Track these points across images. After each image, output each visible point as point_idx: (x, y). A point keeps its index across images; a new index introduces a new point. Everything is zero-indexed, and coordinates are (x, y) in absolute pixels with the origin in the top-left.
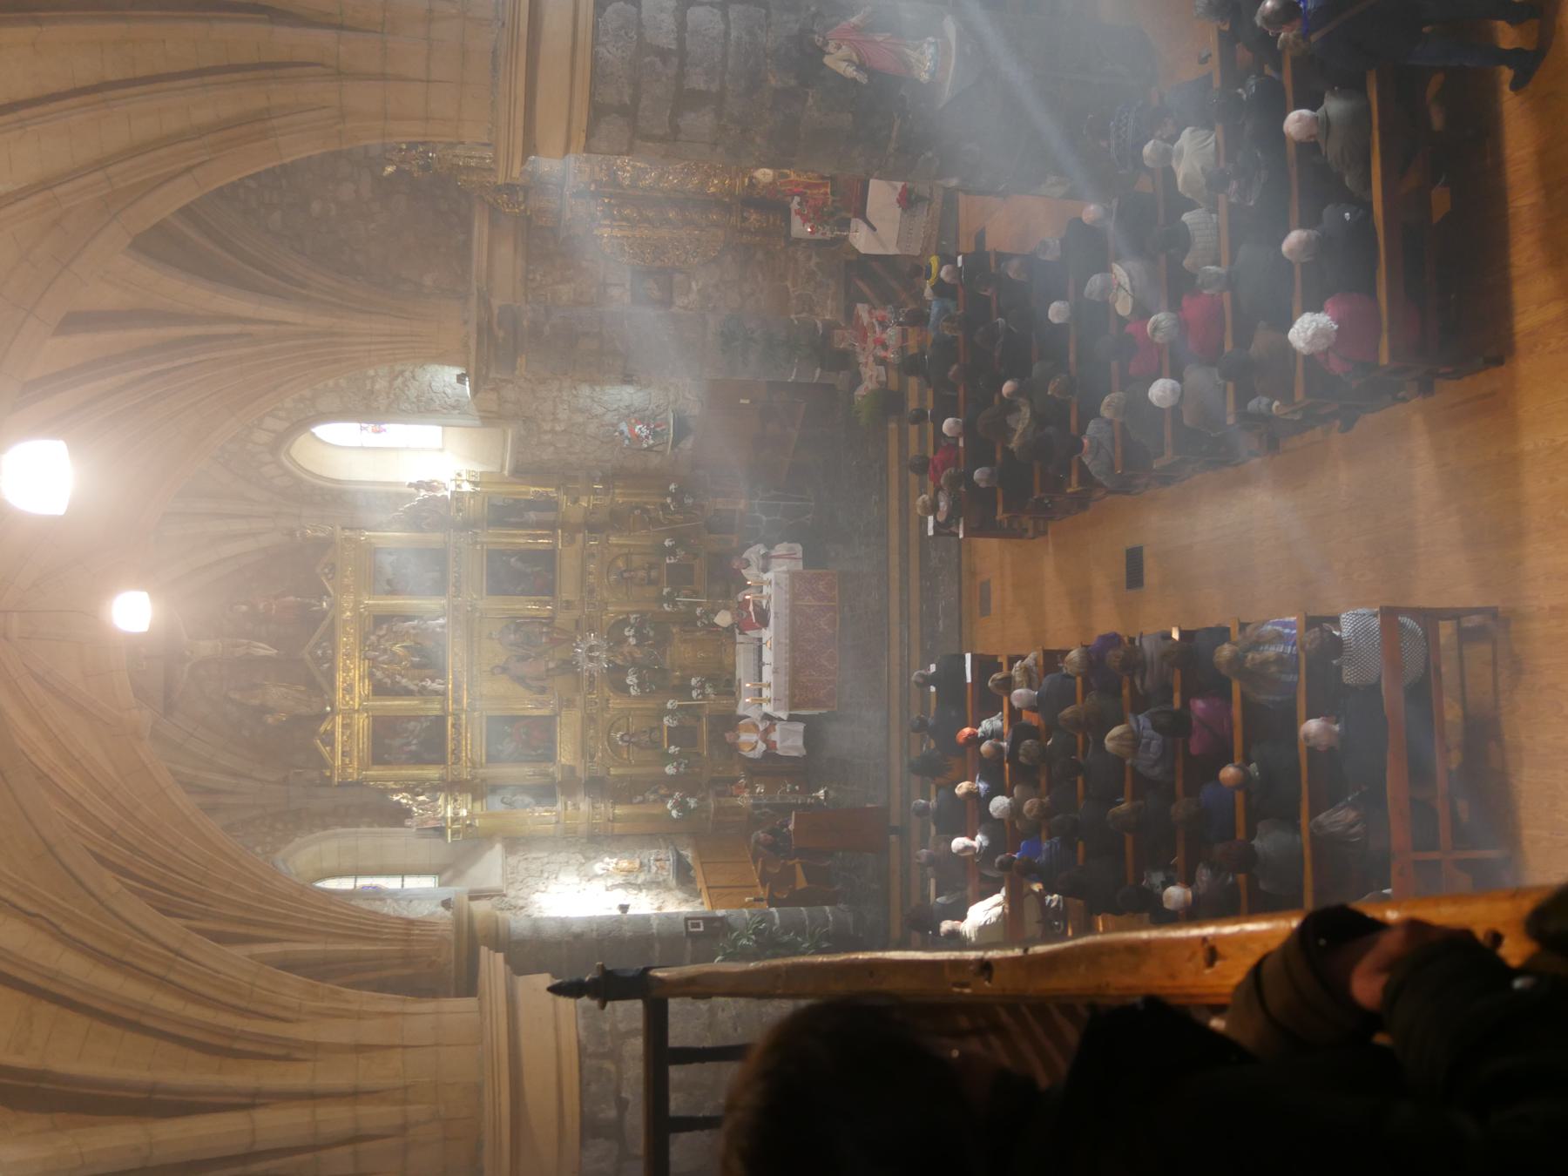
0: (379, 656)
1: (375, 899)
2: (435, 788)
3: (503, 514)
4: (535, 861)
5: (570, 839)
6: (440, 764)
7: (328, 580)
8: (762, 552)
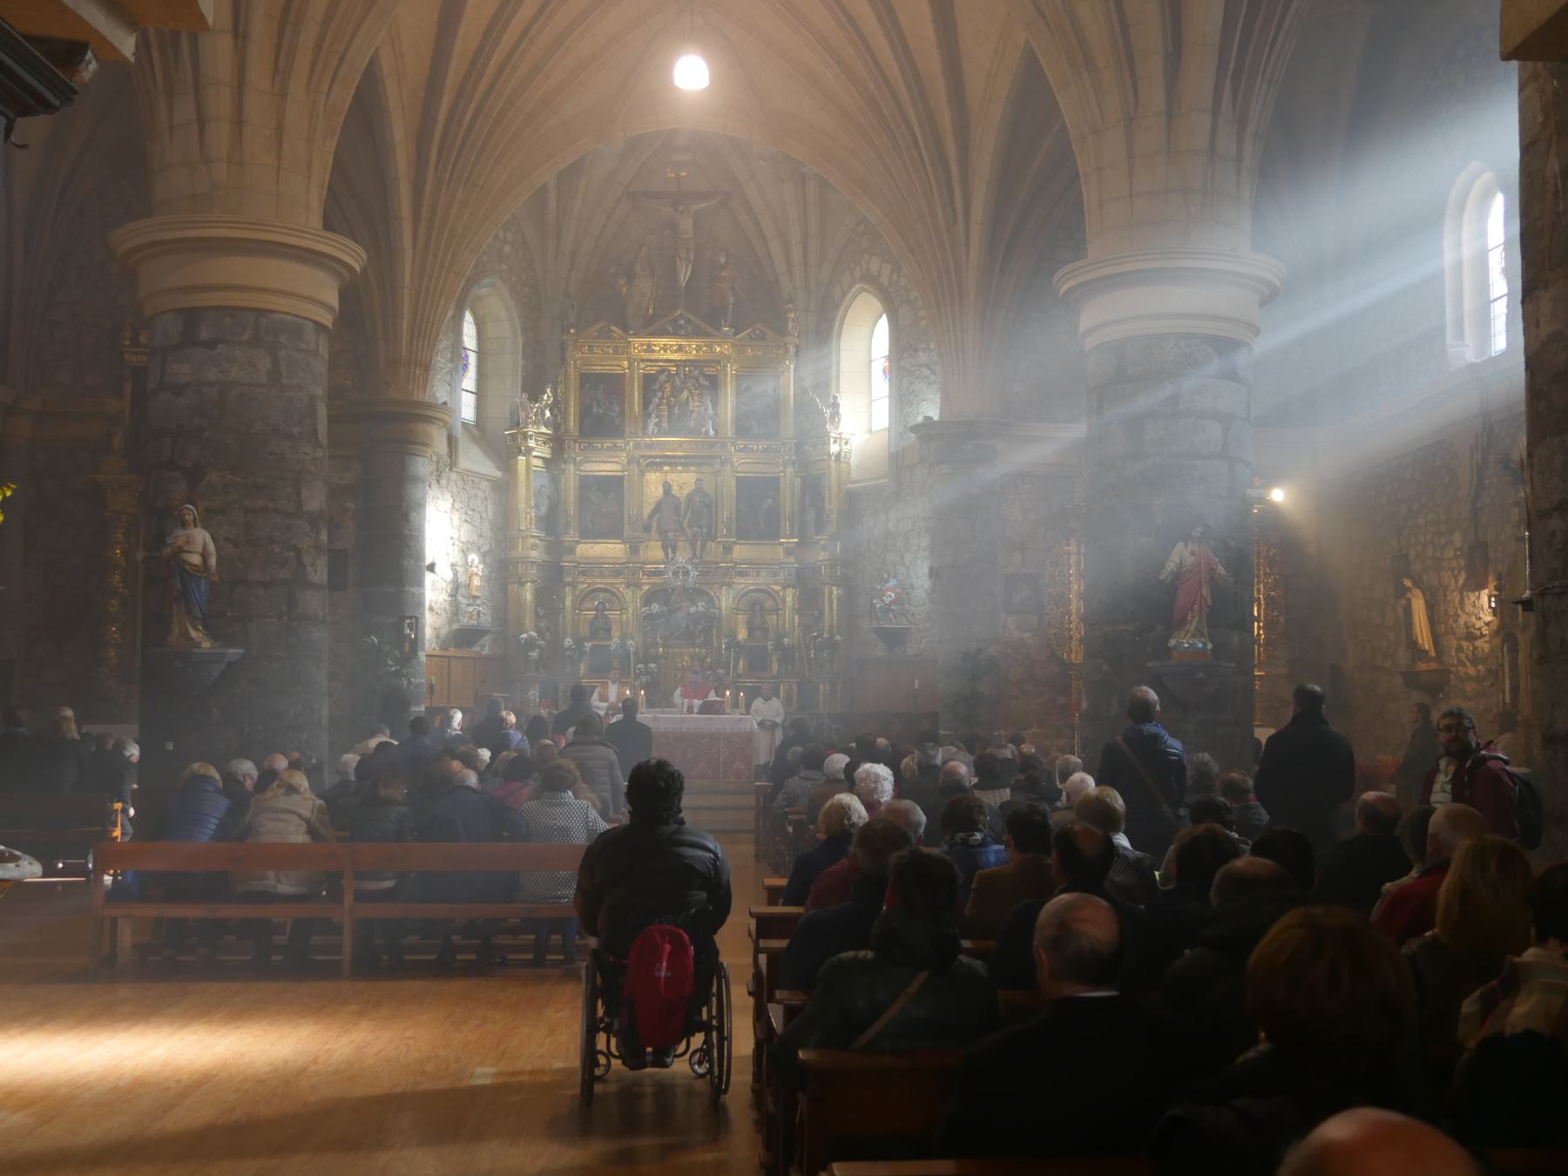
0: (680, 378)
1: (453, 352)
2: (555, 424)
3: (812, 490)
4: (484, 506)
7: (749, 334)
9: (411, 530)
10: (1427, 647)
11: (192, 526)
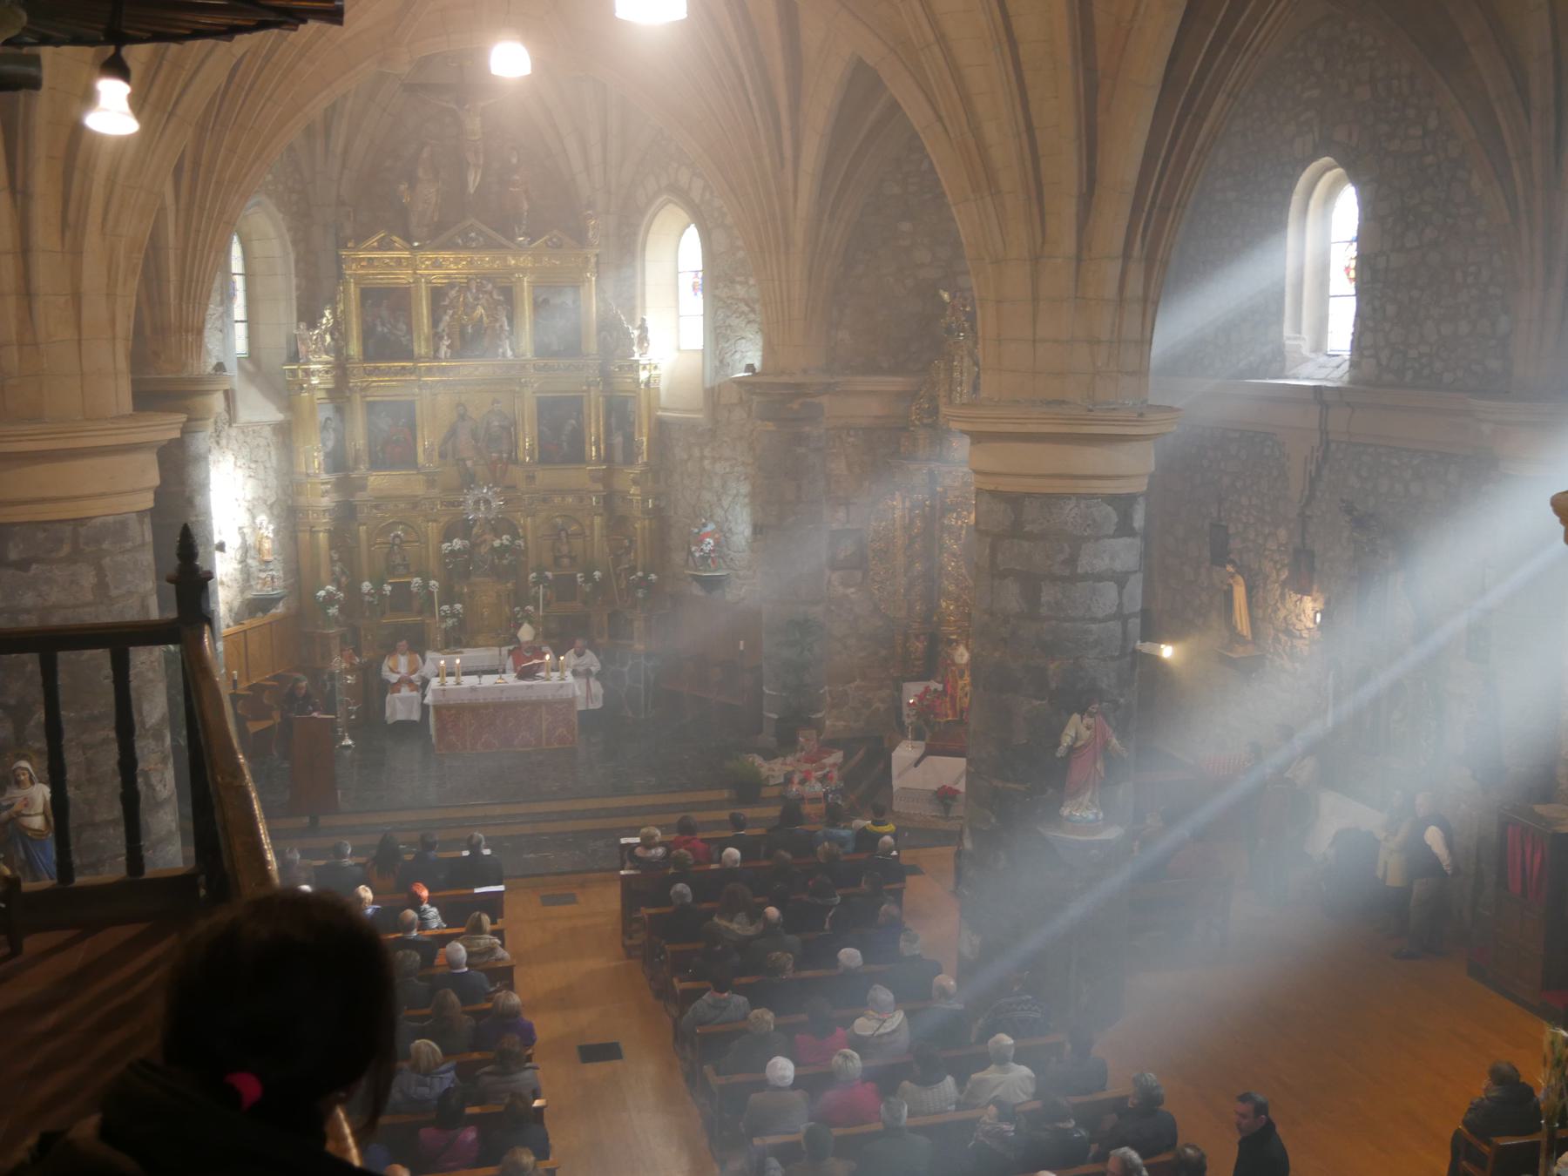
1: (222, 294)
2: (339, 350)
7: (546, 242)
8: (593, 669)
9: (197, 516)
10: (1245, 633)
11: (29, 784)
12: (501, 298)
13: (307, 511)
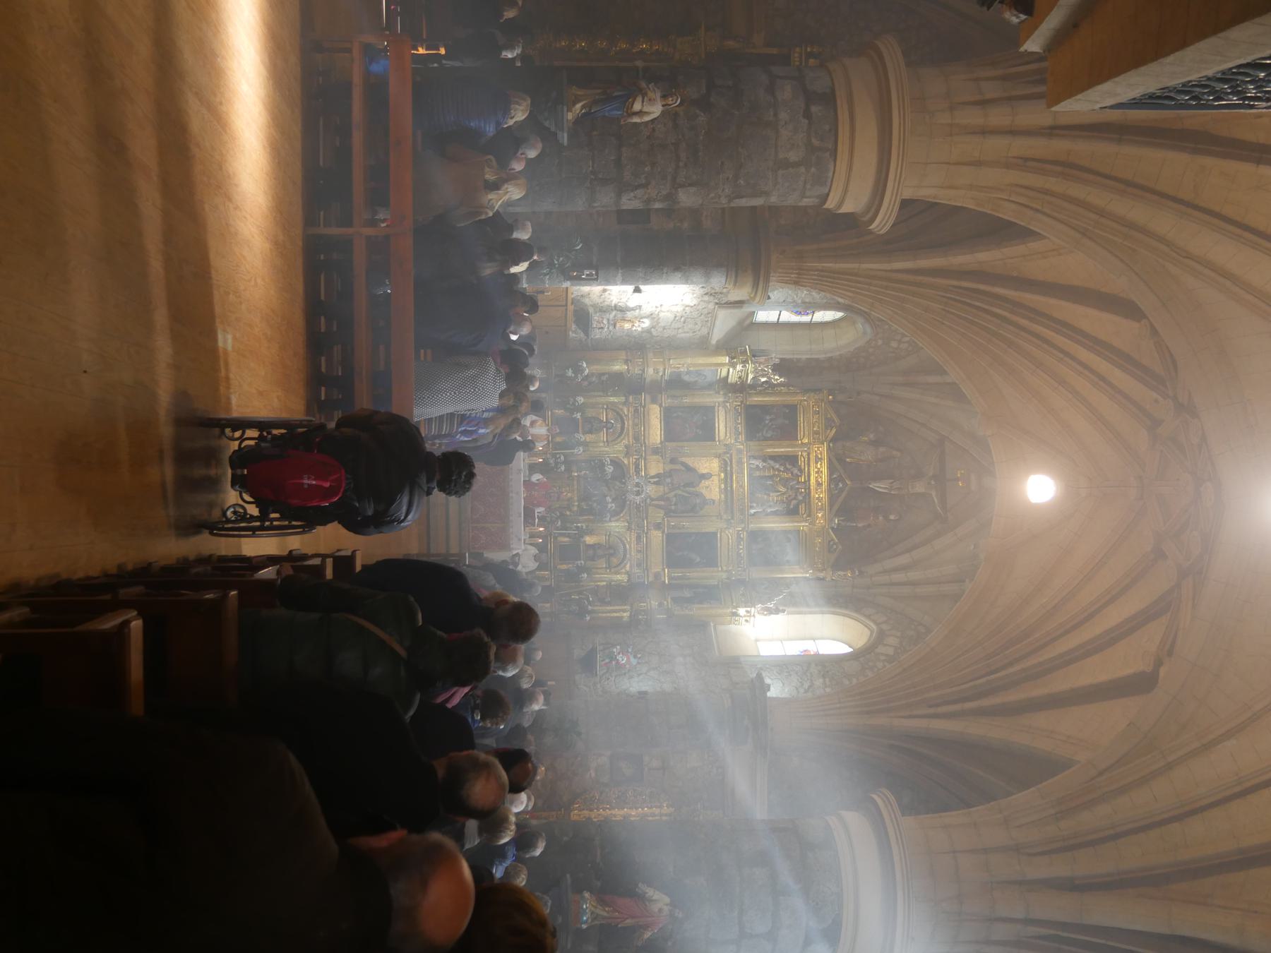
1: (810, 303)
2: (754, 386)
5: (658, 347)
6: (749, 405)
7: (833, 540)
12: (792, 507)
13: (643, 358)
